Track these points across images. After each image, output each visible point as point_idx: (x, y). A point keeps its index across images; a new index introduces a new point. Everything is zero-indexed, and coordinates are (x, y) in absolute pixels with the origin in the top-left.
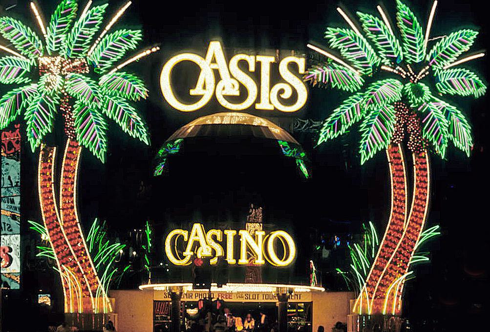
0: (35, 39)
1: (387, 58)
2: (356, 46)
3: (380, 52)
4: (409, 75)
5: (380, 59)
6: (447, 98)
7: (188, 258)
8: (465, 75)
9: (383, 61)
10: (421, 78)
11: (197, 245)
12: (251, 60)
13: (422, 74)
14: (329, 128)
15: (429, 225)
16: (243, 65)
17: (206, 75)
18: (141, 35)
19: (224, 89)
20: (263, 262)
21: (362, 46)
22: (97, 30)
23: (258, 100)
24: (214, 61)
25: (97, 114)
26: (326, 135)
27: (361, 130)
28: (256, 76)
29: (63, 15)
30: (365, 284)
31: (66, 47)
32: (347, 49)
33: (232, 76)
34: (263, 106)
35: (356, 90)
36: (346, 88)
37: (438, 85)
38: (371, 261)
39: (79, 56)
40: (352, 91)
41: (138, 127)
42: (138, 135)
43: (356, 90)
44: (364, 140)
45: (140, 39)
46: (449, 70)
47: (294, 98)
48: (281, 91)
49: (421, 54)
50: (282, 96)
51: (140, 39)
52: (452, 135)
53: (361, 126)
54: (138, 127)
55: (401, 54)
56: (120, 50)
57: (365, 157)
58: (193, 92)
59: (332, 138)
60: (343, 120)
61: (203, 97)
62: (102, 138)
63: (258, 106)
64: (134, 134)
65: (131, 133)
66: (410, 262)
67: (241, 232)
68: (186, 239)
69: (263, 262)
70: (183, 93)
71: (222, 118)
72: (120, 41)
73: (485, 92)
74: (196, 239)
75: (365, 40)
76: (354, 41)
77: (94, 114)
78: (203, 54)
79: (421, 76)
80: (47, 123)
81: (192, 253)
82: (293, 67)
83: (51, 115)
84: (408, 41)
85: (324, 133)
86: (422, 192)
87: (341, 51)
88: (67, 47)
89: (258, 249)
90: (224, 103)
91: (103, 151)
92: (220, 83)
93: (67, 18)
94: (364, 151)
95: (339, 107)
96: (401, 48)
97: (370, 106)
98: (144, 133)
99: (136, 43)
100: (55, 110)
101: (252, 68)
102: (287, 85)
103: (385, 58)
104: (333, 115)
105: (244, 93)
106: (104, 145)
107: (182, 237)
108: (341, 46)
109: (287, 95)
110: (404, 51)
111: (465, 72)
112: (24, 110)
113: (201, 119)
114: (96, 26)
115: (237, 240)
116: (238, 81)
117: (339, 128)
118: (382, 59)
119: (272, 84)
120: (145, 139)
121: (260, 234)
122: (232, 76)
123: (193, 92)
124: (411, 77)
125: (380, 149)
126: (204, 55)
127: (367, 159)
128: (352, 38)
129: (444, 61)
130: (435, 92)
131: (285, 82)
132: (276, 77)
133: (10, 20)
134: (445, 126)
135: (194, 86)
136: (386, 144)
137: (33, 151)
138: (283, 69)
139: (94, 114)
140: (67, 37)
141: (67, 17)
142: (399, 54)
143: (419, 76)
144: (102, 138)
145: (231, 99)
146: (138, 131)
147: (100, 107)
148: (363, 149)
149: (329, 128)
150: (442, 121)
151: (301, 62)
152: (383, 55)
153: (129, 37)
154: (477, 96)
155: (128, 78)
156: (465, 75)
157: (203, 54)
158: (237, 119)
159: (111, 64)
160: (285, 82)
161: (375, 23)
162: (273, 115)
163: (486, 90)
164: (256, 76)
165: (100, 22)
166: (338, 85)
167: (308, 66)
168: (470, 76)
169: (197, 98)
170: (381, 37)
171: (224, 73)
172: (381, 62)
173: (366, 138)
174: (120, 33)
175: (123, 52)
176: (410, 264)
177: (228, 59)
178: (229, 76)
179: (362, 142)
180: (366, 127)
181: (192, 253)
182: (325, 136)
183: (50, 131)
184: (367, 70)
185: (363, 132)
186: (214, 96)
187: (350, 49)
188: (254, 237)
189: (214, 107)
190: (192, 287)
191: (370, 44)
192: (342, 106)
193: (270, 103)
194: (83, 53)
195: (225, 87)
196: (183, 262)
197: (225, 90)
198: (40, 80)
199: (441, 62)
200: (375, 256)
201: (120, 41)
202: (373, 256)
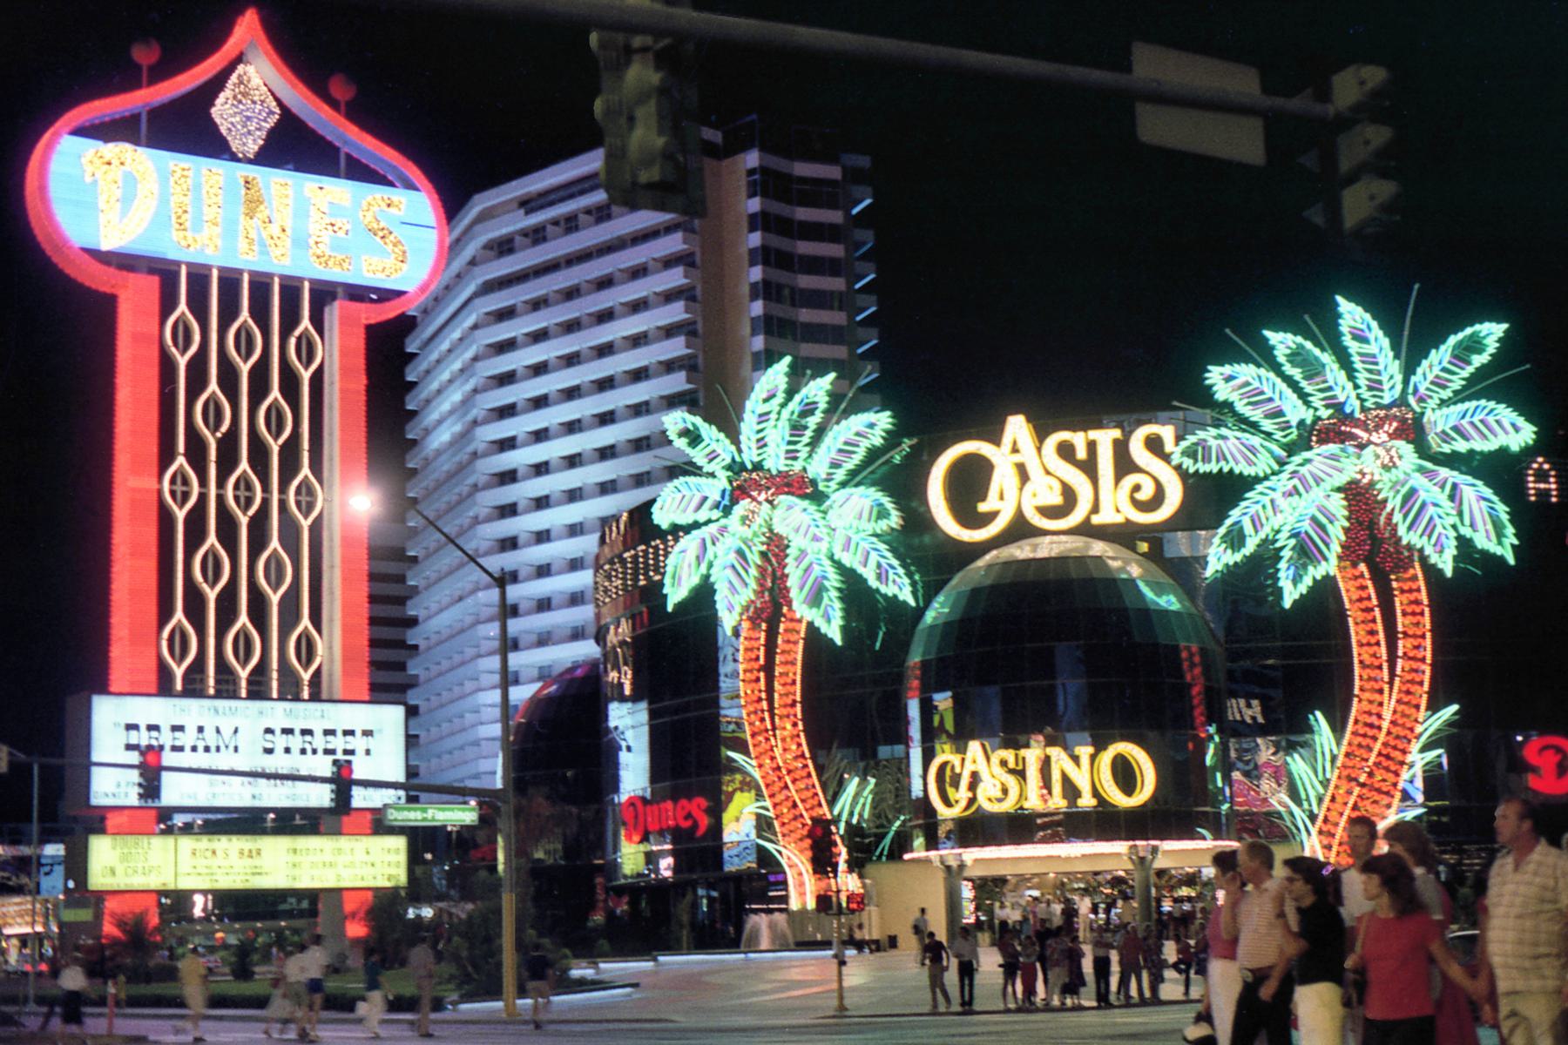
1: (1327, 407)
2: (1262, 393)
3: (1310, 399)
6: (1453, 461)
11: (975, 779)
12: (1079, 440)
15: (1434, 707)
16: (1066, 451)
17: (1003, 478)
19: (1035, 495)
20: (1093, 802)
23: (1095, 509)
24: (1015, 450)
26: (1218, 558)
28: (1089, 467)
30: (1314, 831)
33: (1048, 473)
34: (1105, 517)
36: (1248, 471)
48: (1137, 488)
49: (1392, 388)
58: (983, 507)
60: (1248, 528)
63: (1096, 520)
69: (1093, 802)
70: (967, 513)
71: (1035, 548)
72: (858, 434)
75: (1278, 381)
78: (995, 438)
82: (1154, 445)
89: (1081, 779)
92: (1028, 486)
101: (1081, 454)
109: (1146, 493)
112: (710, 565)
113: (994, 553)
118: (1316, 409)
122: (1048, 473)
123: (983, 507)
130: (1423, 451)
131: (1138, 470)
132: (1124, 465)
156: (1486, 411)
157: (995, 438)
158: (1062, 548)
160: (1138, 470)
162: (1123, 535)
164: (1089, 467)
169: (991, 516)
170: (1366, 349)
171: (1034, 469)
178: (1043, 471)
189: (1020, 529)
190: (355, 766)
201: (858, 434)
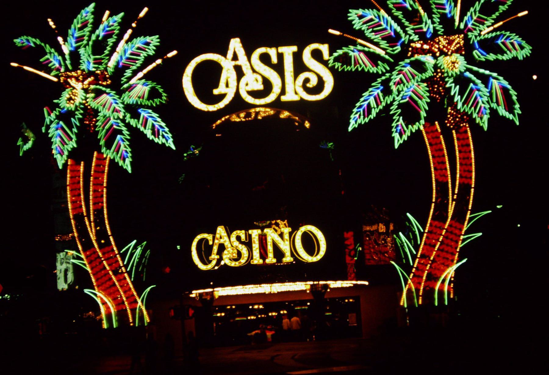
0: (54, 56)
1: (416, 34)
2: (381, 25)
3: (407, 29)
4: (442, 47)
5: (408, 36)
7: (214, 262)
8: (505, 37)
9: (411, 38)
10: (455, 48)
11: (222, 248)
12: (272, 52)
13: (456, 44)
14: (359, 113)
16: (265, 59)
18: (159, 40)
19: (247, 85)
21: (387, 25)
22: (115, 40)
23: (283, 92)
25: (120, 125)
27: (391, 113)
28: (279, 68)
29: (80, 29)
31: (86, 60)
32: (371, 30)
33: (254, 71)
34: (287, 98)
35: (384, 71)
37: (476, 53)
38: (417, 247)
39: (99, 68)
40: (380, 73)
41: (164, 133)
42: (164, 141)
43: (384, 71)
44: (396, 123)
45: (158, 44)
46: (487, 35)
47: (321, 84)
48: (307, 80)
50: (308, 85)
51: (158, 44)
52: (496, 104)
53: (391, 108)
54: (164, 133)
55: (431, 27)
56: (138, 58)
57: (398, 140)
58: (216, 92)
59: (363, 123)
61: (228, 94)
62: (127, 148)
63: (284, 98)
64: (160, 141)
65: (156, 140)
66: (460, 245)
67: (266, 230)
68: (211, 243)
73: (530, 52)
74: (222, 241)
75: (389, 19)
76: (377, 20)
77: (117, 124)
79: (455, 46)
80: (71, 139)
81: (218, 257)
82: (317, 55)
83: (75, 130)
84: (437, 12)
85: (354, 119)
86: (467, 169)
87: (365, 32)
88: (86, 60)
90: (250, 100)
91: (128, 161)
93: (84, 31)
94: (397, 134)
95: (367, 90)
96: (430, 20)
97: (399, 86)
98: (169, 138)
99: (155, 48)
100: (78, 124)
101: (274, 60)
102: (312, 73)
103: (414, 35)
104: (362, 99)
105: (268, 85)
106: (130, 155)
107: (207, 241)
108: (364, 27)
109: (314, 82)
110: (433, 23)
111: (505, 35)
114: (113, 36)
115: (263, 239)
116: (260, 74)
117: (369, 113)
118: (410, 35)
119: (296, 75)
120: (171, 144)
121: (287, 230)
122: (254, 71)
123: (216, 92)
124: (445, 49)
125: (414, 131)
126: (224, 54)
127: (401, 142)
128: (375, 17)
129: (481, 26)
131: (309, 70)
133: (28, 38)
134: (485, 95)
135: (217, 86)
136: (420, 125)
137: (61, 167)
138: (307, 57)
139: (117, 124)
140: (86, 50)
141: (84, 30)
142: (429, 28)
143: (453, 46)
144: (127, 148)
145: (255, 94)
146: (163, 136)
147: (121, 117)
148: (396, 132)
149: (359, 113)
150: (481, 91)
151: (324, 48)
152: (410, 32)
153: (148, 44)
154: (520, 58)
155: (148, 85)
156: (505, 37)
159: (131, 73)
160: (309, 70)
161: (360, 111)
163: (531, 50)
164: (279, 68)
165: (116, 32)
166: (365, 68)
167: (331, 51)
168: (511, 38)
169: (222, 97)
171: (246, 69)
172: (409, 39)
173: (398, 121)
174: (139, 42)
175: (142, 59)
176: (461, 248)
177: (249, 55)
178: (251, 71)
179: (394, 124)
180: (397, 109)
181: (218, 257)
182: (356, 122)
183: (75, 146)
184: (394, 49)
185: (394, 114)
186: (237, 94)
187: (375, 29)
188: (281, 235)
191: (395, 22)
192: (370, 89)
193: (296, 93)
194: (103, 64)
195: (248, 83)
196: (209, 267)
197: (249, 85)
198: (62, 95)
199: (477, 28)
200: (421, 241)
201: (139, 48)
202: (419, 243)
